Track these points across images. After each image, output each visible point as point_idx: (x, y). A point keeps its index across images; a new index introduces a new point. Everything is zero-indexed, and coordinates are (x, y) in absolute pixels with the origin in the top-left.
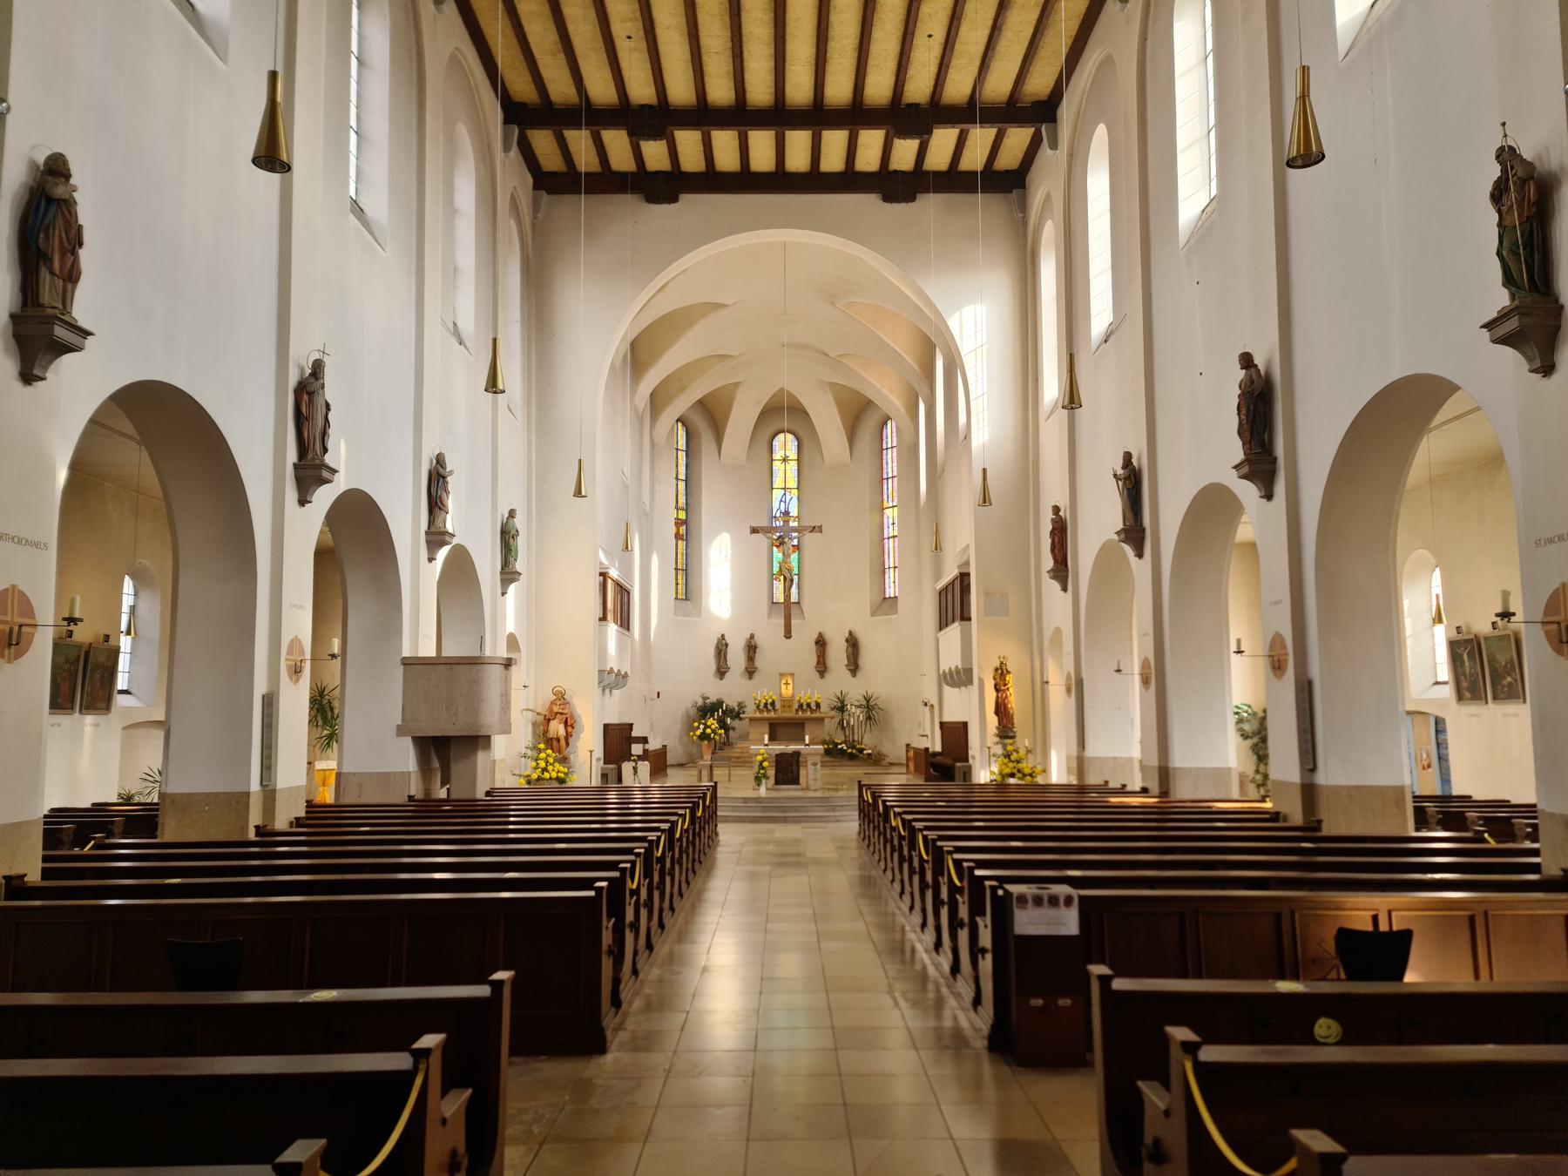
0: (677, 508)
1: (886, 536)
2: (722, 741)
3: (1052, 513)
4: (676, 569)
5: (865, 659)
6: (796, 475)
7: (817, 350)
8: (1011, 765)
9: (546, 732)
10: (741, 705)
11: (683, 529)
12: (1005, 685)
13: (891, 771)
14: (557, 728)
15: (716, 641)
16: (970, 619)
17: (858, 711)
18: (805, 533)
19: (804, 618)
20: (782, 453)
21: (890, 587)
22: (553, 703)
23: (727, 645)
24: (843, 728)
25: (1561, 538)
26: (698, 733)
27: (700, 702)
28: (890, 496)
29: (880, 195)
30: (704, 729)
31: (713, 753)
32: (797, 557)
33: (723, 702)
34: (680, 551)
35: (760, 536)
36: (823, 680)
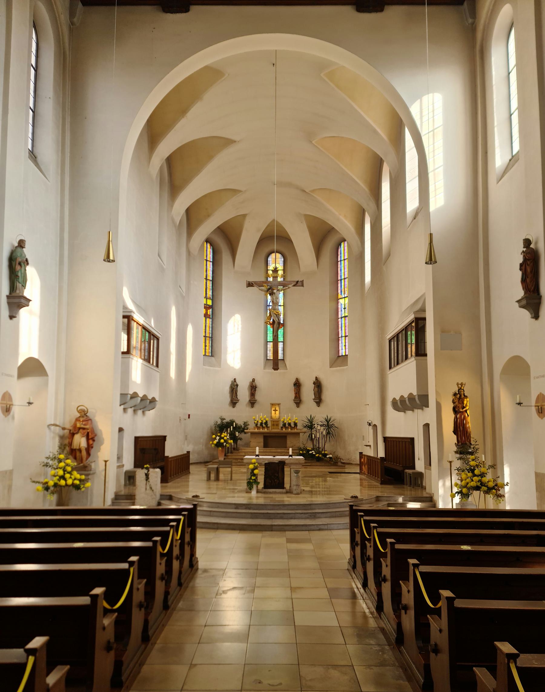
0: (206, 297)
1: (340, 316)
2: (233, 447)
3: (522, 246)
4: (205, 336)
5: (326, 395)
6: (283, 265)
7: (297, 188)
8: (475, 478)
9: (71, 444)
10: (246, 424)
11: (210, 312)
12: (463, 408)
13: (347, 471)
14: (80, 441)
15: (230, 383)
16: (426, 355)
17: (322, 428)
18: (290, 286)
19: (287, 369)
20: (274, 265)
21: (342, 349)
22: (77, 420)
23: (237, 385)
24: (312, 440)
25: (543, 376)
26: (215, 442)
27: (219, 422)
28: (343, 291)
29: (355, 7)
30: (219, 440)
31: (225, 455)
32: (282, 331)
33: (234, 422)
34: (208, 325)
35: (255, 289)
36: (298, 409)
